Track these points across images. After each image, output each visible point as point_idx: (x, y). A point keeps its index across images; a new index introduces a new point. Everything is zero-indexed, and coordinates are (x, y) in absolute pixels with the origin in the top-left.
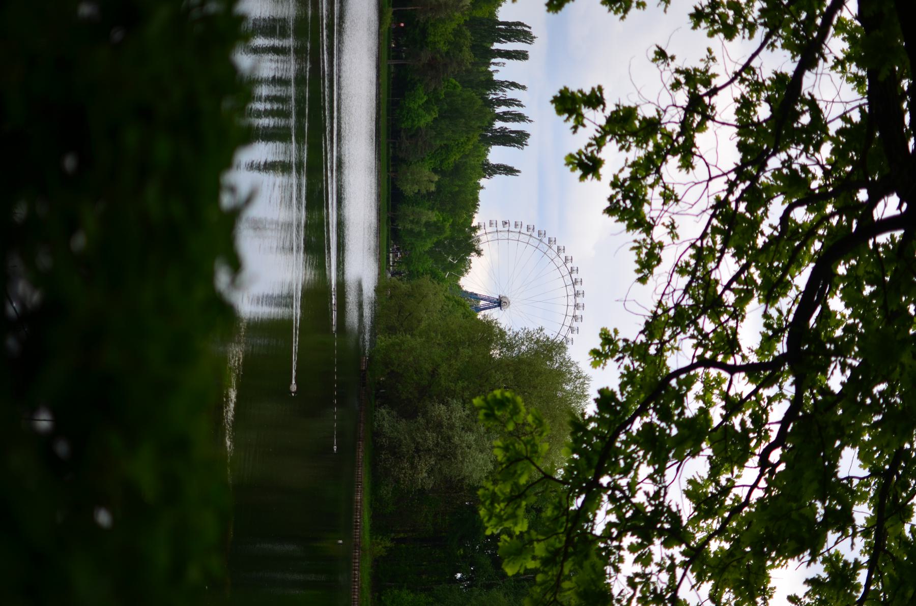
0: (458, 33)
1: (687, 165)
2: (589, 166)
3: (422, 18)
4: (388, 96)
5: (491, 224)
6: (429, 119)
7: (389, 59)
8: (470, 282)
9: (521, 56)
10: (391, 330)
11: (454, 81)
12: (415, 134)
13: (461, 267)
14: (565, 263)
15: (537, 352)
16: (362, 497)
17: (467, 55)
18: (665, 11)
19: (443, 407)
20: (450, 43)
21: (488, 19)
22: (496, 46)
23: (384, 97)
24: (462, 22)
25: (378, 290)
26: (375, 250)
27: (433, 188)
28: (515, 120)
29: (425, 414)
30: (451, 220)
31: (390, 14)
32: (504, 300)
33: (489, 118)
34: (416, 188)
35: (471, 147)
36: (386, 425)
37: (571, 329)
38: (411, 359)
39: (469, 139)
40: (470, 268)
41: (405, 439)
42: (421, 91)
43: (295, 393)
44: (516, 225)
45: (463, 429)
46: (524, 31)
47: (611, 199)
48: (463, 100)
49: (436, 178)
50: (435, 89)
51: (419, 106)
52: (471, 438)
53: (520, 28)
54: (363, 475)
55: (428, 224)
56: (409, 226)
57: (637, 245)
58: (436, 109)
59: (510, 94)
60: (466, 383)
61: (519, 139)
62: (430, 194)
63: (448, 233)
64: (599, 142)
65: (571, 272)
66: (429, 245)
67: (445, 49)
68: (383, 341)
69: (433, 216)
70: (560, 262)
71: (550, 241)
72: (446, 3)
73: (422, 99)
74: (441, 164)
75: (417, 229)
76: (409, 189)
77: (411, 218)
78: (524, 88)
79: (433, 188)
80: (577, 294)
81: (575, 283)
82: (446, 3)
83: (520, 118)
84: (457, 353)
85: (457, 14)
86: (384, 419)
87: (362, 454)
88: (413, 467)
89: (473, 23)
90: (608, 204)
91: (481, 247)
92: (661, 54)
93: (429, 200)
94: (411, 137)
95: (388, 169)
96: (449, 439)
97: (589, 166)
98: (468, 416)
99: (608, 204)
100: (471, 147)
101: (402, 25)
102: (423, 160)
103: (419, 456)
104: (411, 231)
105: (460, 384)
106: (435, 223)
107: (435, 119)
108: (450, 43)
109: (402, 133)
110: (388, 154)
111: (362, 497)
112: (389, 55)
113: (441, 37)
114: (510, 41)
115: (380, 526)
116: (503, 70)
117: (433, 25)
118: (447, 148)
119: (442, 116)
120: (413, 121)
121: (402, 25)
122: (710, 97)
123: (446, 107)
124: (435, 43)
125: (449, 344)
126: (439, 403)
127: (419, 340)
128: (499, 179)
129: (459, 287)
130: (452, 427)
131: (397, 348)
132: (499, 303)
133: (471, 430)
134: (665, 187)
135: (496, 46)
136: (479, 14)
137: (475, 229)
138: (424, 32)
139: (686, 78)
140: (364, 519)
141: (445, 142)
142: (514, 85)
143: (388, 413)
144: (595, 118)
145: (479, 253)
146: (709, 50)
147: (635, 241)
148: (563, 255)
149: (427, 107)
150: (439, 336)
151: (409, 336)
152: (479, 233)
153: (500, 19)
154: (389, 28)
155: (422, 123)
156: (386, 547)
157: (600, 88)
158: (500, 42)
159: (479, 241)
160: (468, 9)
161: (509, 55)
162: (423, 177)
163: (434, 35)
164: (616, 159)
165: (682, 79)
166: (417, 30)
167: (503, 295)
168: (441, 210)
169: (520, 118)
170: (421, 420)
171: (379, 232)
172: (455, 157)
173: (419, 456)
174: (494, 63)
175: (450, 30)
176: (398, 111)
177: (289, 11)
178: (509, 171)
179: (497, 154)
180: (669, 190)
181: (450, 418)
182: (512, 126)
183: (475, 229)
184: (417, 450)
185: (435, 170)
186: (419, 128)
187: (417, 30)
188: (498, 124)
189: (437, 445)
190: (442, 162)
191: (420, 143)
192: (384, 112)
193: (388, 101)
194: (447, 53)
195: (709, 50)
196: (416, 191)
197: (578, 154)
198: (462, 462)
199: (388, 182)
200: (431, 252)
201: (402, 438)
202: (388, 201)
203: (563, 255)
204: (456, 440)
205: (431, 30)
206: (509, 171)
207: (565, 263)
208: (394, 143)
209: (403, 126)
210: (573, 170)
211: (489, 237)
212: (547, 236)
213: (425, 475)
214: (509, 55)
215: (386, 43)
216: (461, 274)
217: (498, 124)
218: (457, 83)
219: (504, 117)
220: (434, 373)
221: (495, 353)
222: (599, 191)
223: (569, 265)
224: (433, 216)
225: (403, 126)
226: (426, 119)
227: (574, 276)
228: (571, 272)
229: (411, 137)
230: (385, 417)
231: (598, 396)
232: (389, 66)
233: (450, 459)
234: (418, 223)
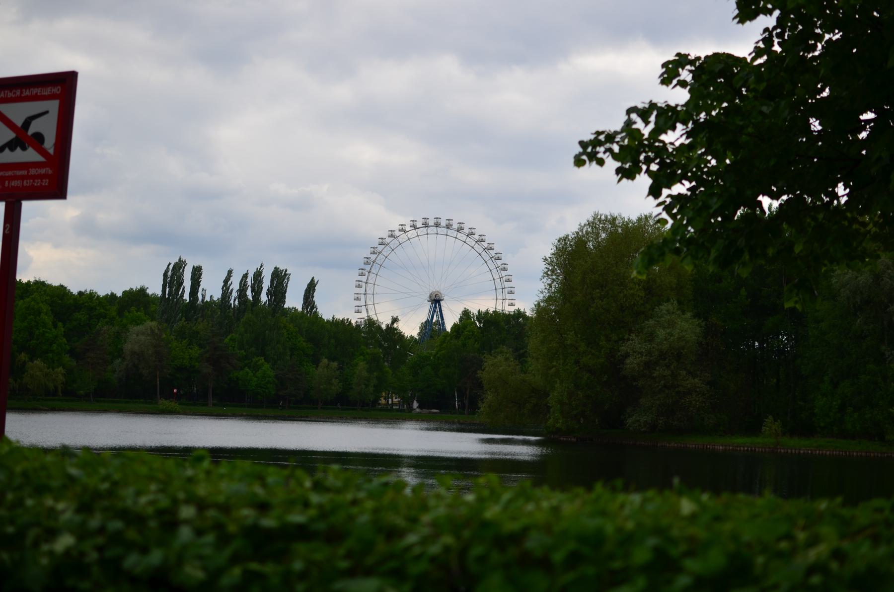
6: (266, 366)
7: (207, 405)
8: (410, 328)
9: (197, 273)
14: (405, 231)
16: (720, 444)
28: (261, 282)
30: (363, 347)
32: (433, 297)
35: (291, 326)
37: (460, 230)
44: (359, 286)
52: (661, 333)
53: (169, 273)
54: (694, 442)
56: (371, 389)
58: (255, 359)
59: (235, 286)
61: (280, 279)
65: (415, 227)
70: (403, 237)
71: (374, 253)
77: (363, 386)
78: (230, 273)
79: (335, 364)
80: (437, 225)
81: (426, 225)
83: (258, 275)
86: (638, 421)
100: (291, 326)
115: (754, 429)
116: (211, 289)
123: (253, 349)
124: (191, 358)
128: (318, 298)
132: (436, 301)
135: (186, 297)
140: (742, 442)
142: (226, 281)
148: (397, 233)
153: (159, 293)
155: (271, 373)
158: (182, 295)
162: (322, 373)
167: (427, 297)
169: (258, 275)
177: (339, 585)
178: (311, 287)
179: (294, 300)
181: (641, 353)
182: (266, 284)
185: (316, 362)
188: (264, 298)
201: (658, 402)
203: (388, 240)
206: (311, 287)
207: (405, 231)
212: (369, 255)
213: (696, 380)
216: (403, 336)
217: (264, 298)
218: (229, 337)
219: (257, 291)
223: (408, 228)
227: (419, 225)
228: (415, 227)
232: (214, 405)
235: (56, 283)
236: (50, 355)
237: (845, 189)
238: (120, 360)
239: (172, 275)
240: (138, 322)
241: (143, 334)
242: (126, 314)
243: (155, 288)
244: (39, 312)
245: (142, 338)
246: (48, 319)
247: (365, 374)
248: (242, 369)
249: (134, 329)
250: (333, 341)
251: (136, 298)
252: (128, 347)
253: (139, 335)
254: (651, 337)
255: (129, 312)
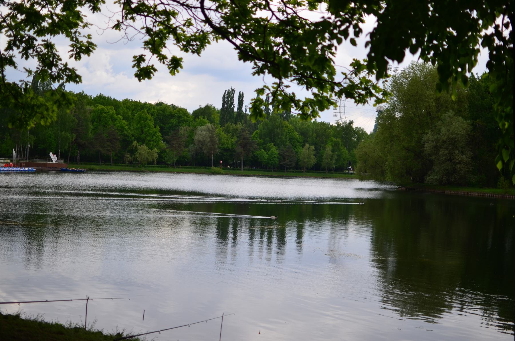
0: (227, 131)
1: (174, 14)
2: (175, 64)
3: (218, 151)
4: (261, 171)
5: (335, 116)
9: (241, 96)
10: (383, 173)
11: (254, 134)
12: (282, 156)
13: (360, 133)
15: (398, 91)
16: (476, 192)
17: (239, 126)
18: (92, 25)
19: (426, 145)
20: (233, 135)
21: (221, 114)
22: (236, 110)
23: (261, 173)
24: (221, 128)
25: (362, 179)
26: (348, 181)
27: (313, 147)
29: (430, 155)
31: (215, 168)
32: (379, 109)
33: (275, 115)
34: (313, 157)
36: (436, 177)
38: (399, 162)
39: (287, 127)
40: (360, 128)
41: (444, 166)
42: (258, 153)
43: (276, 217)
45: (439, 134)
46: (228, 94)
47: (193, 52)
48: (264, 129)
49: (307, 145)
50: (258, 144)
51: (267, 154)
52: (443, 130)
54: (463, 191)
55: (333, 151)
56: (334, 161)
57: (215, 39)
60: (414, 132)
62: (316, 149)
63: (339, 140)
64: (162, 58)
66: (345, 150)
67: (235, 138)
68: (389, 177)
69: (329, 148)
72: (210, 138)
73: (263, 152)
74: (300, 143)
75: (336, 157)
76: (313, 160)
77: (329, 160)
79: (313, 147)
82: (210, 138)
84: (397, 136)
85: (217, 131)
87: (452, 191)
88: (459, 163)
89: (222, 123)
90: (196, 54)
91: (348, 122)
92: (117, 26)
93: (320, 150)
94: (284, 158)
95: (301, 172)
96: (444, 142)
97: (175, 64)
98: (432, 131)
99: (196, 54)
101: (221, 162)
102: (297, 153)
103: (454, 159)
104: (336, 160)
105: (414, 135)
106: (333, 146)
107: (274, 145)
108: (233, 135)
109: (282, 163)
110: (293, 172)
111: (476, 192)
112: (238, 170)
113: (230, 141)
114: (233, 102)
117: (222, 145)
118: (291, 139)
119: (273, 141)
120: (275, 157)
121: (221, 162)
122: (133, 3)
123: (268, 139)
124: (232, 144)
125: (391, 141)
126: (424, 147)
127: (389, 157)
129: (371, 134)
130: (437, 140)
131: (392, 170)
133: (440, 129)
134: (184, 25)
135: (236, 110)
136: (217, 119)
137: (338, 124)
138: (226, 150)
139: (130, 14)
140: (488, 192)
141: (288, 140)
143: (429, 176)
144: (151, 59)
145: (351, 122)
146: (115, 3)
147: (214, 40)
149: (267, 149)
150: (387, 146)
151: (386, 163)
152: (341, 122)
154: (223, 169)
155: (276, 152)
156: (505, 180)
157: (135, 57)
158: (233, 108)
159: (345, 123)
160: (214, 125)
161: (241, 103)
162: (306, 152)
163: (228, 144)
164: (171, 48)
165: (129, 16)
166: (225, 153)
168: (326, 143)
170: (433, 158)
171: (336, 178)
172: (296, 134)
173: (454, 159)
174: (246, 112)
175: (225, 136)
176: (269, 165)
180: (186, 23)
181: (432, 141)
183: (338, 124)
184: (450, 160)
185: (303, 146)
186: (279, 154)
187: (225, 153)
189: (447, 149)
190: (298, 142)
191: (287, 154)
192: (270, 174)
193: (263, 171)
194: (238, 137)
195: (115, 3)
196: (314, 157)
197: (169, 69)
198: (457, 134)
199: (309, 172)
200: (349, 150)
202: (319, 173)
204: (444, 138)
205: (225, 146)
208: (287, 168)
209: (277, 163)
210: (178, 72)
211: (343, 117)
213: (464, 156)
214: (241, 103)
215: (231, 171)
218: (255, 132)
220: (408, 149)
221: (398, 115)
222: (188, 58)
224: (329, 148)
225: (277, 163)
226: (274, 149)
229: (284, 158)
230: (431, 178)
231: (242, 61)
232: (244, 170)
233: (455, 141)
234: (332, 157)
235: (169, 103)
236: (152, 143)
237: (497, 44)
238: (192, 145)
239: (227, 97)
240: (202, 124)
241: (205, 131)
242: (197, 119)
243: (218, 105)
244: (146, 119)
245: (204, 133)
246: (151, 123)
247: (330, 153)
248: (259, 150)
249: (200, 128)
250: (315, 134)
251: (205, 112)
252: (196, 138)
253: (202, 132)
254: (439, 132)
255: (198, 118)
